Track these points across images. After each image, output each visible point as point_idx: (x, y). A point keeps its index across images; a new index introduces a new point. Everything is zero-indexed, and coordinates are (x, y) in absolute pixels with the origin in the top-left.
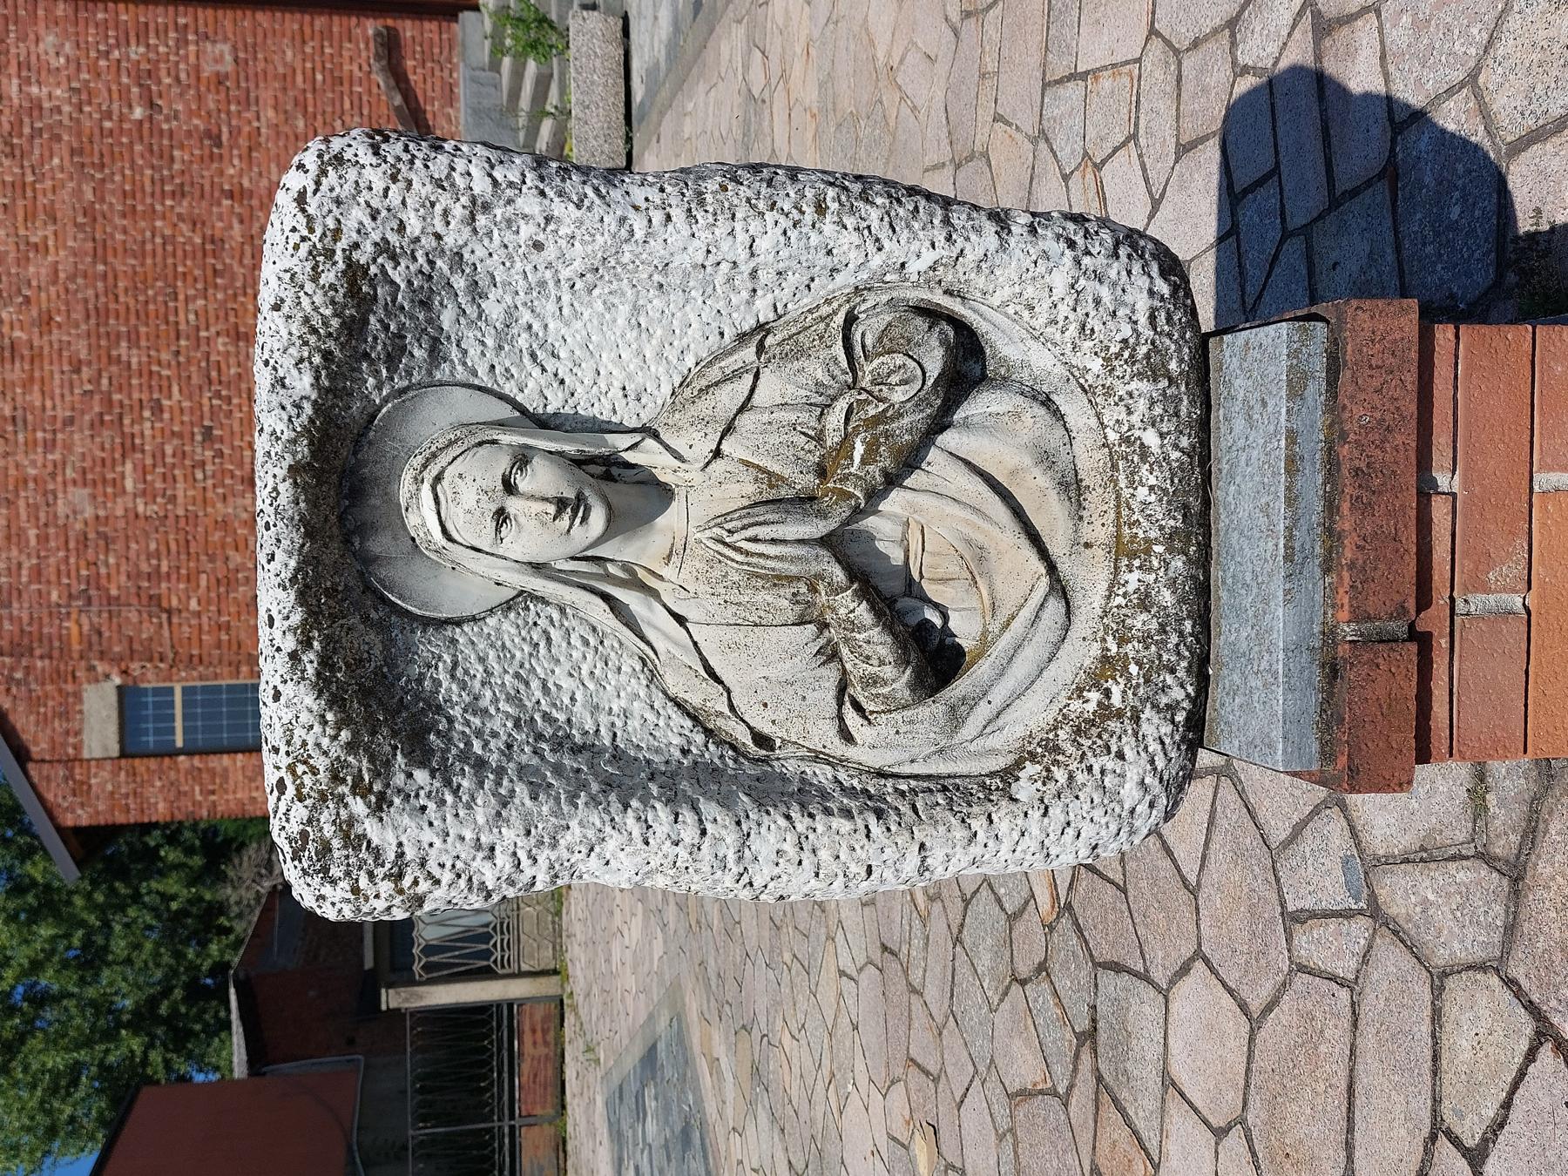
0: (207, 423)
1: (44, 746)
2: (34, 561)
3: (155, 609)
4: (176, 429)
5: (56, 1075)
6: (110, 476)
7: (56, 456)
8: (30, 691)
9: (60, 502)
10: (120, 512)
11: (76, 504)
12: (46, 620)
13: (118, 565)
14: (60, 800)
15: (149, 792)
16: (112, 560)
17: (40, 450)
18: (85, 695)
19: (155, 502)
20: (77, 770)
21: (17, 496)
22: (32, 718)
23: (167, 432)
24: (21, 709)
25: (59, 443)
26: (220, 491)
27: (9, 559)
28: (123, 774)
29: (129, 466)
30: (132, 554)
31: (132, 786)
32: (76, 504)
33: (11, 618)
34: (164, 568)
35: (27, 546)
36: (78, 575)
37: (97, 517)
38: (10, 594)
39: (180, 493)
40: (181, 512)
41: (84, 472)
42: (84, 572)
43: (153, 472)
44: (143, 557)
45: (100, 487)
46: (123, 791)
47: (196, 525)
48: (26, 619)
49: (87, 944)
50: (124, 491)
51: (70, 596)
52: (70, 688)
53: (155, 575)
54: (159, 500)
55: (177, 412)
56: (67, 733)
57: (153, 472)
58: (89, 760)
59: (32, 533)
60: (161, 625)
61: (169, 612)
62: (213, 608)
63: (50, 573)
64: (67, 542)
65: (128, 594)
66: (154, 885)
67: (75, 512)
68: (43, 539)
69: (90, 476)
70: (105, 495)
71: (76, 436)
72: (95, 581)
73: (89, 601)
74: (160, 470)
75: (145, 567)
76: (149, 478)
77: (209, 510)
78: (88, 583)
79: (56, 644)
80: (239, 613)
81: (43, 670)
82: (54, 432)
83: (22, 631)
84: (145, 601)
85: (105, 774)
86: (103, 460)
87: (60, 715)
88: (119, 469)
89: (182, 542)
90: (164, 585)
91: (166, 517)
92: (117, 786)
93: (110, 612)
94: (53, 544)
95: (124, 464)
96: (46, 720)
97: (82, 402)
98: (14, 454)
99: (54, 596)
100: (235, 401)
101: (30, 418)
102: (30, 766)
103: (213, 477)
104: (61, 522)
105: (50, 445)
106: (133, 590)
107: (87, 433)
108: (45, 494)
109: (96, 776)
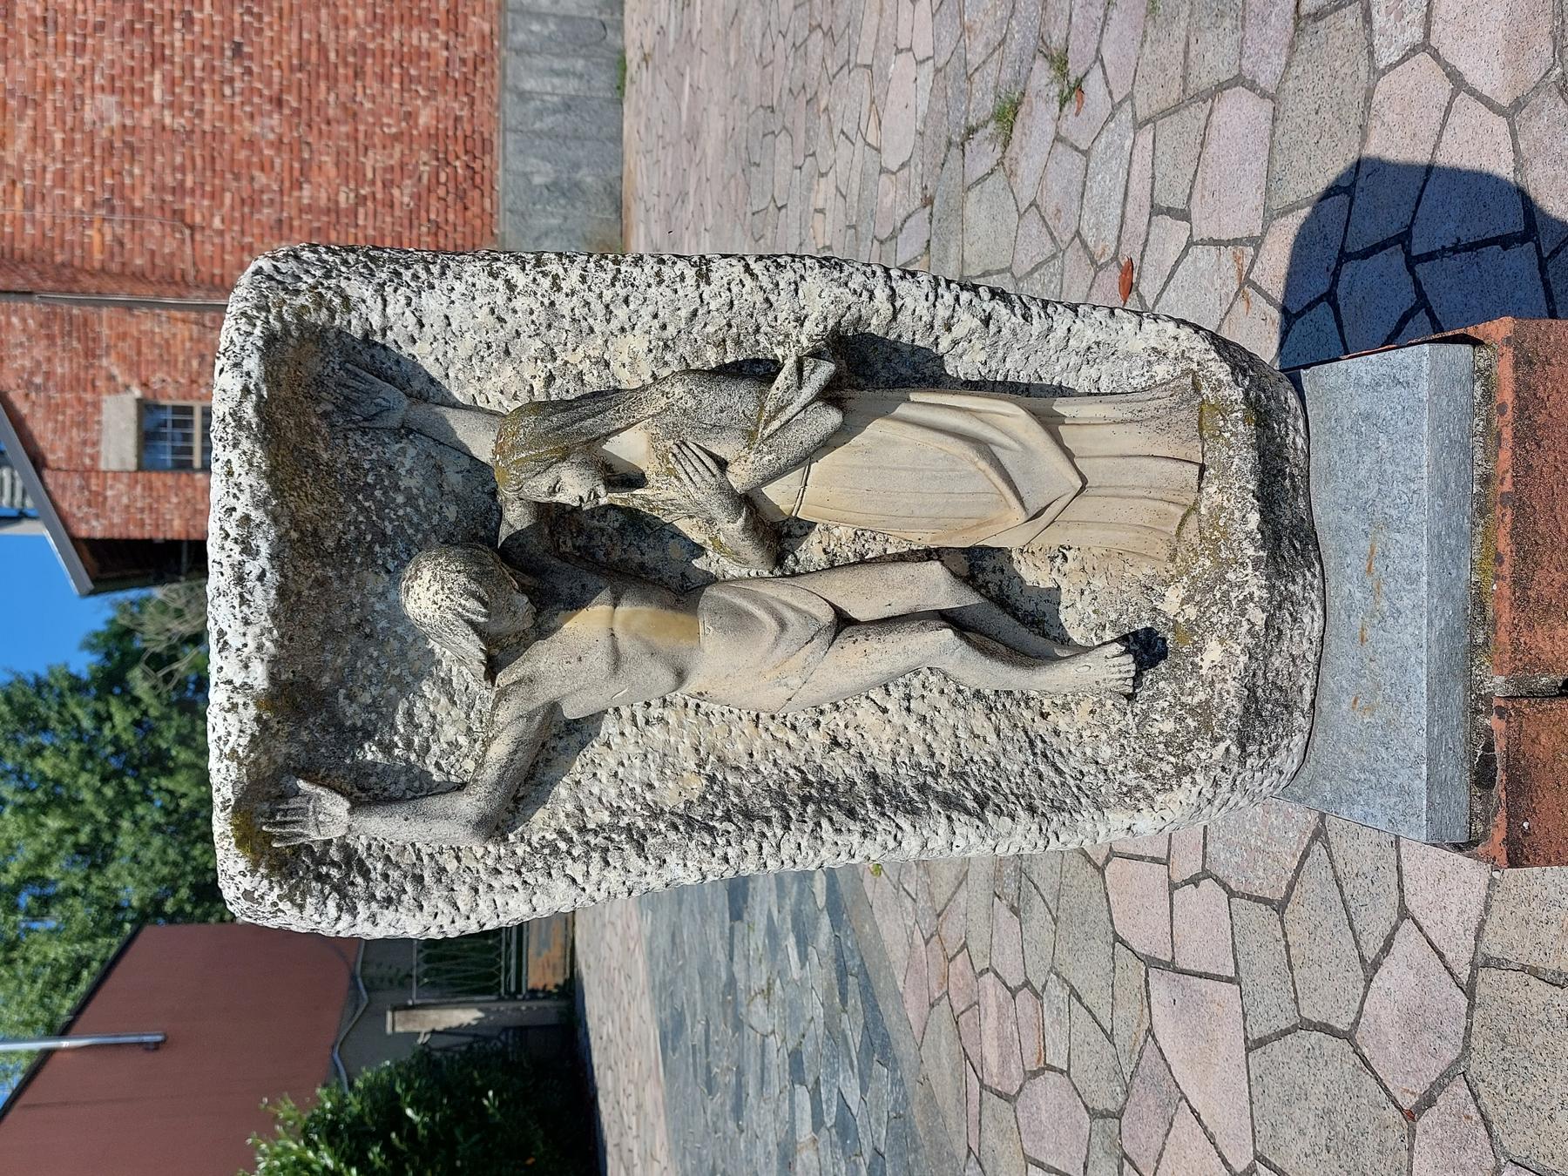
0: (237, 39)
1: (61, 454)
2: (59, 166)
3: (178, 224)
4: (206, 42)
5: (58, 969)
6: (138, 85)
7: (85, 61)
8: (49, 398)
9: (87, 108)
10: (146, 123)
11: (103, 110)
12: (68, 226)
13: (143, 176)
14: (75, 510)
15: (165, 507)
16: (137, 171)
17: (69, 53)
18: (104, 406)
19: (182, 115)
20: (93, 481)
21: (45, 98)
22: (50, 425)
23: (197, 46)
24: (39, 415)
25: (89, 48)
26: (248, 109)
27: (34, 161)
28: (139, 488)
29: (158, 76)
30: (157, 167)
31: (148, 500)
32: (103, 110)
33: (33, 222)
34: (189, 183)
35: (53, 149)
36: (103, 184)
37: (124, 126)
38: (34, 196)
39: (207, 108)
40: (207, 128)
41: (113, 78)
42: (108, 181)
43: (181, 85)
44: (168, 171)
45: (128, 94)
46: (139, 505)
47: (222, 142)
48: (48, 221)
49: (96, 835)
50: (151, 102)
51: (94, 204)
52: (88, 397)
53: (179, 190)
54: (187, 113)
55: (207, 25)
56: (84, 443)
57: (181, 85)
58: (105, 472)
59: (58, 136)
60: (183, 240)
61: (192, 228)
62: (236, 228)
63: (75, 178)
64: (92, 148)
65: (152, 206)
66: (164, 782)
67: (102, 120)
68: (69, 143)
69: (118, 84)
70: (133, 103)
71: (106, 43)
72: (118, 190)
73: (112, 210)
74: (188, 83)
75: (169, 181)
76: (177, 90)
77: (236, 127)
78: (112, 192)
79: (78, 252)
80: (262, 236)
81: (63, 376)
82: (85, 36)
83: (44, 235)
84: (168, 214)
85: (121, 487)
86: (132, 68)
87: (78, 425)
88: (147, 79)
89: (208, 158)
90: (188, 200)
91: (192, 131)
92: (133, 500)
93: (133, 223)
94: (78, 149)
95: (152, 73)
96: (63, 429)
97: (113, 8)
98: (44, 55)
99: (78, 202)
100: (266, 19)
101: (61, 20)
102: (46, 473)
103: (242, 94)
104: (87, 128)
105: (79, 49)
106: (157, 203)
107: (117, 39)
108: (73, 97)
109: (112, 487)
